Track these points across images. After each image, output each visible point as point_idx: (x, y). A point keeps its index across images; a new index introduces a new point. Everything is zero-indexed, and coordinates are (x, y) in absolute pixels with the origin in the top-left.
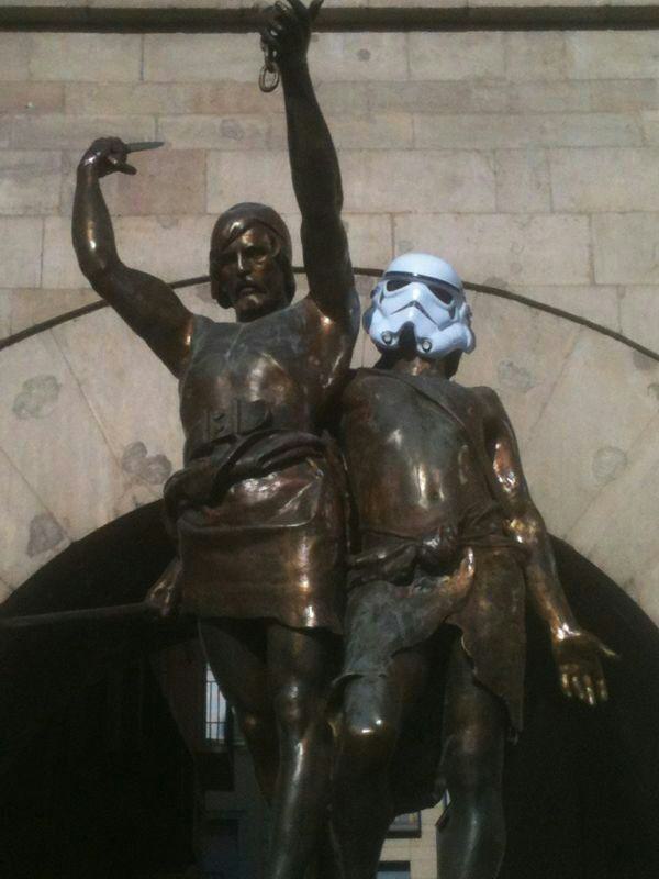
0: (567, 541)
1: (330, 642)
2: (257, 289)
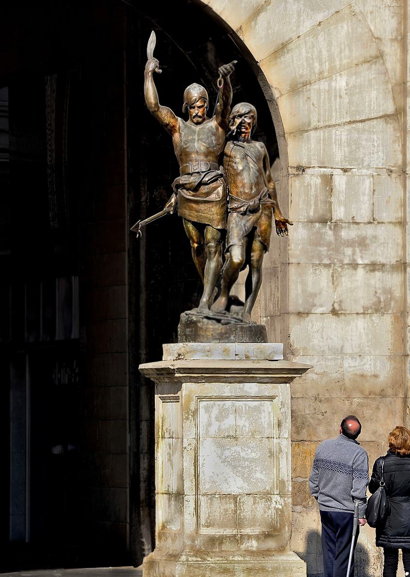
0: (210, 5)
1: (224, 234)
2: (200, 117)
